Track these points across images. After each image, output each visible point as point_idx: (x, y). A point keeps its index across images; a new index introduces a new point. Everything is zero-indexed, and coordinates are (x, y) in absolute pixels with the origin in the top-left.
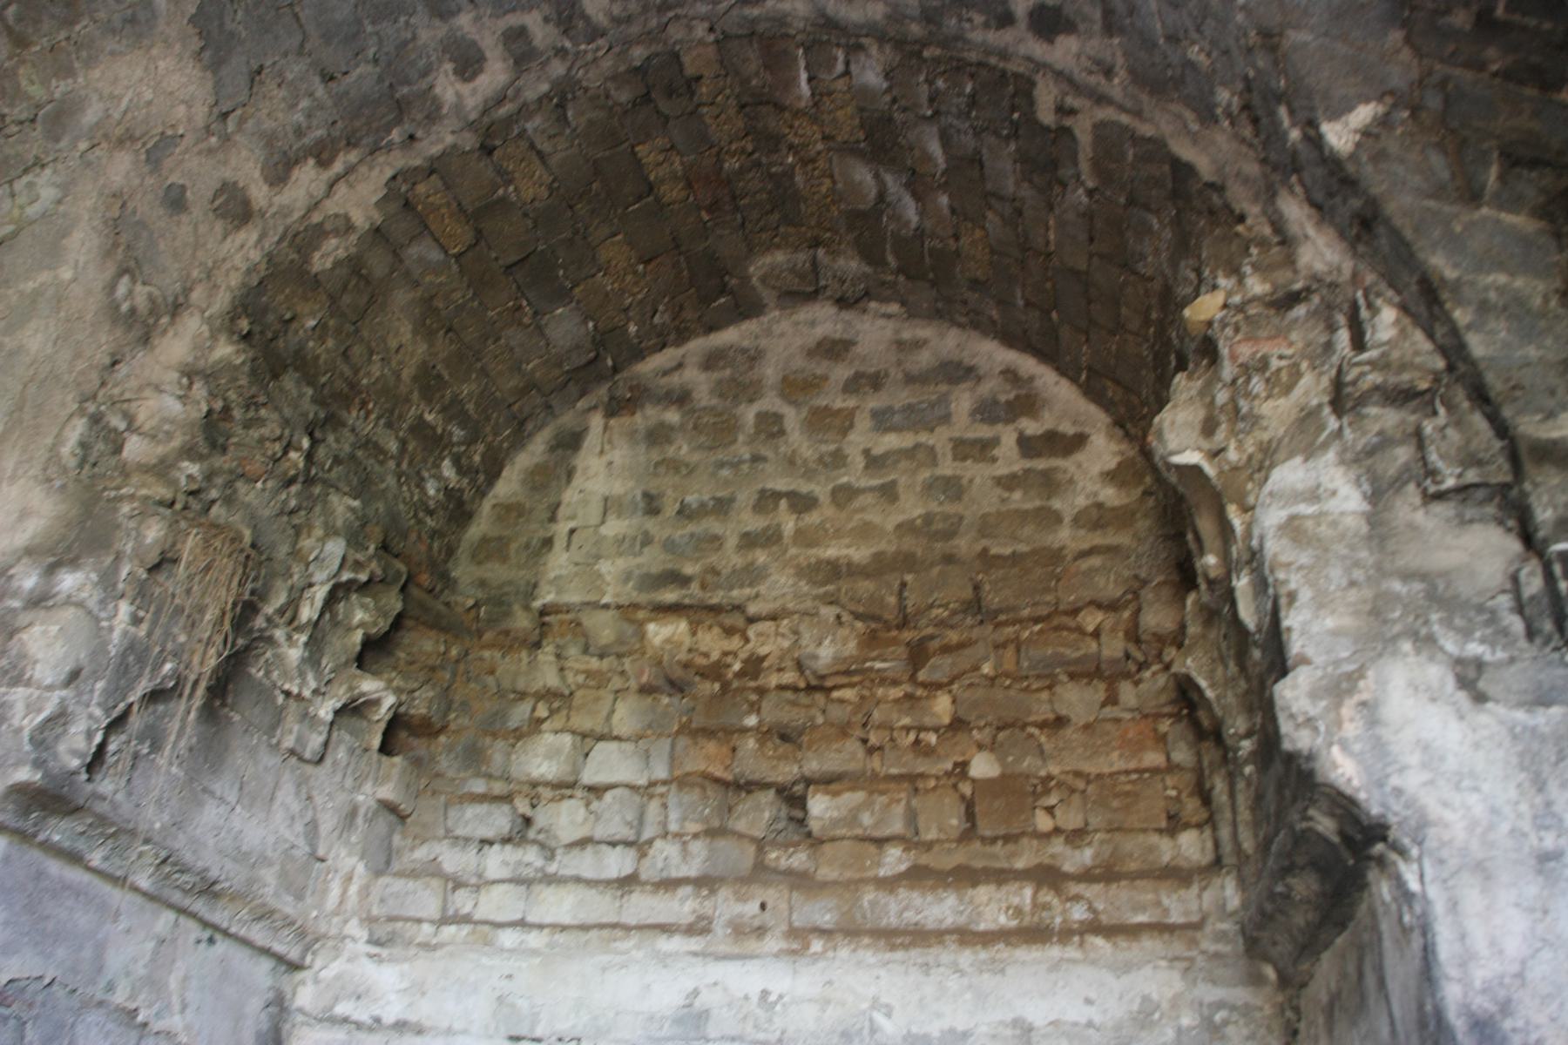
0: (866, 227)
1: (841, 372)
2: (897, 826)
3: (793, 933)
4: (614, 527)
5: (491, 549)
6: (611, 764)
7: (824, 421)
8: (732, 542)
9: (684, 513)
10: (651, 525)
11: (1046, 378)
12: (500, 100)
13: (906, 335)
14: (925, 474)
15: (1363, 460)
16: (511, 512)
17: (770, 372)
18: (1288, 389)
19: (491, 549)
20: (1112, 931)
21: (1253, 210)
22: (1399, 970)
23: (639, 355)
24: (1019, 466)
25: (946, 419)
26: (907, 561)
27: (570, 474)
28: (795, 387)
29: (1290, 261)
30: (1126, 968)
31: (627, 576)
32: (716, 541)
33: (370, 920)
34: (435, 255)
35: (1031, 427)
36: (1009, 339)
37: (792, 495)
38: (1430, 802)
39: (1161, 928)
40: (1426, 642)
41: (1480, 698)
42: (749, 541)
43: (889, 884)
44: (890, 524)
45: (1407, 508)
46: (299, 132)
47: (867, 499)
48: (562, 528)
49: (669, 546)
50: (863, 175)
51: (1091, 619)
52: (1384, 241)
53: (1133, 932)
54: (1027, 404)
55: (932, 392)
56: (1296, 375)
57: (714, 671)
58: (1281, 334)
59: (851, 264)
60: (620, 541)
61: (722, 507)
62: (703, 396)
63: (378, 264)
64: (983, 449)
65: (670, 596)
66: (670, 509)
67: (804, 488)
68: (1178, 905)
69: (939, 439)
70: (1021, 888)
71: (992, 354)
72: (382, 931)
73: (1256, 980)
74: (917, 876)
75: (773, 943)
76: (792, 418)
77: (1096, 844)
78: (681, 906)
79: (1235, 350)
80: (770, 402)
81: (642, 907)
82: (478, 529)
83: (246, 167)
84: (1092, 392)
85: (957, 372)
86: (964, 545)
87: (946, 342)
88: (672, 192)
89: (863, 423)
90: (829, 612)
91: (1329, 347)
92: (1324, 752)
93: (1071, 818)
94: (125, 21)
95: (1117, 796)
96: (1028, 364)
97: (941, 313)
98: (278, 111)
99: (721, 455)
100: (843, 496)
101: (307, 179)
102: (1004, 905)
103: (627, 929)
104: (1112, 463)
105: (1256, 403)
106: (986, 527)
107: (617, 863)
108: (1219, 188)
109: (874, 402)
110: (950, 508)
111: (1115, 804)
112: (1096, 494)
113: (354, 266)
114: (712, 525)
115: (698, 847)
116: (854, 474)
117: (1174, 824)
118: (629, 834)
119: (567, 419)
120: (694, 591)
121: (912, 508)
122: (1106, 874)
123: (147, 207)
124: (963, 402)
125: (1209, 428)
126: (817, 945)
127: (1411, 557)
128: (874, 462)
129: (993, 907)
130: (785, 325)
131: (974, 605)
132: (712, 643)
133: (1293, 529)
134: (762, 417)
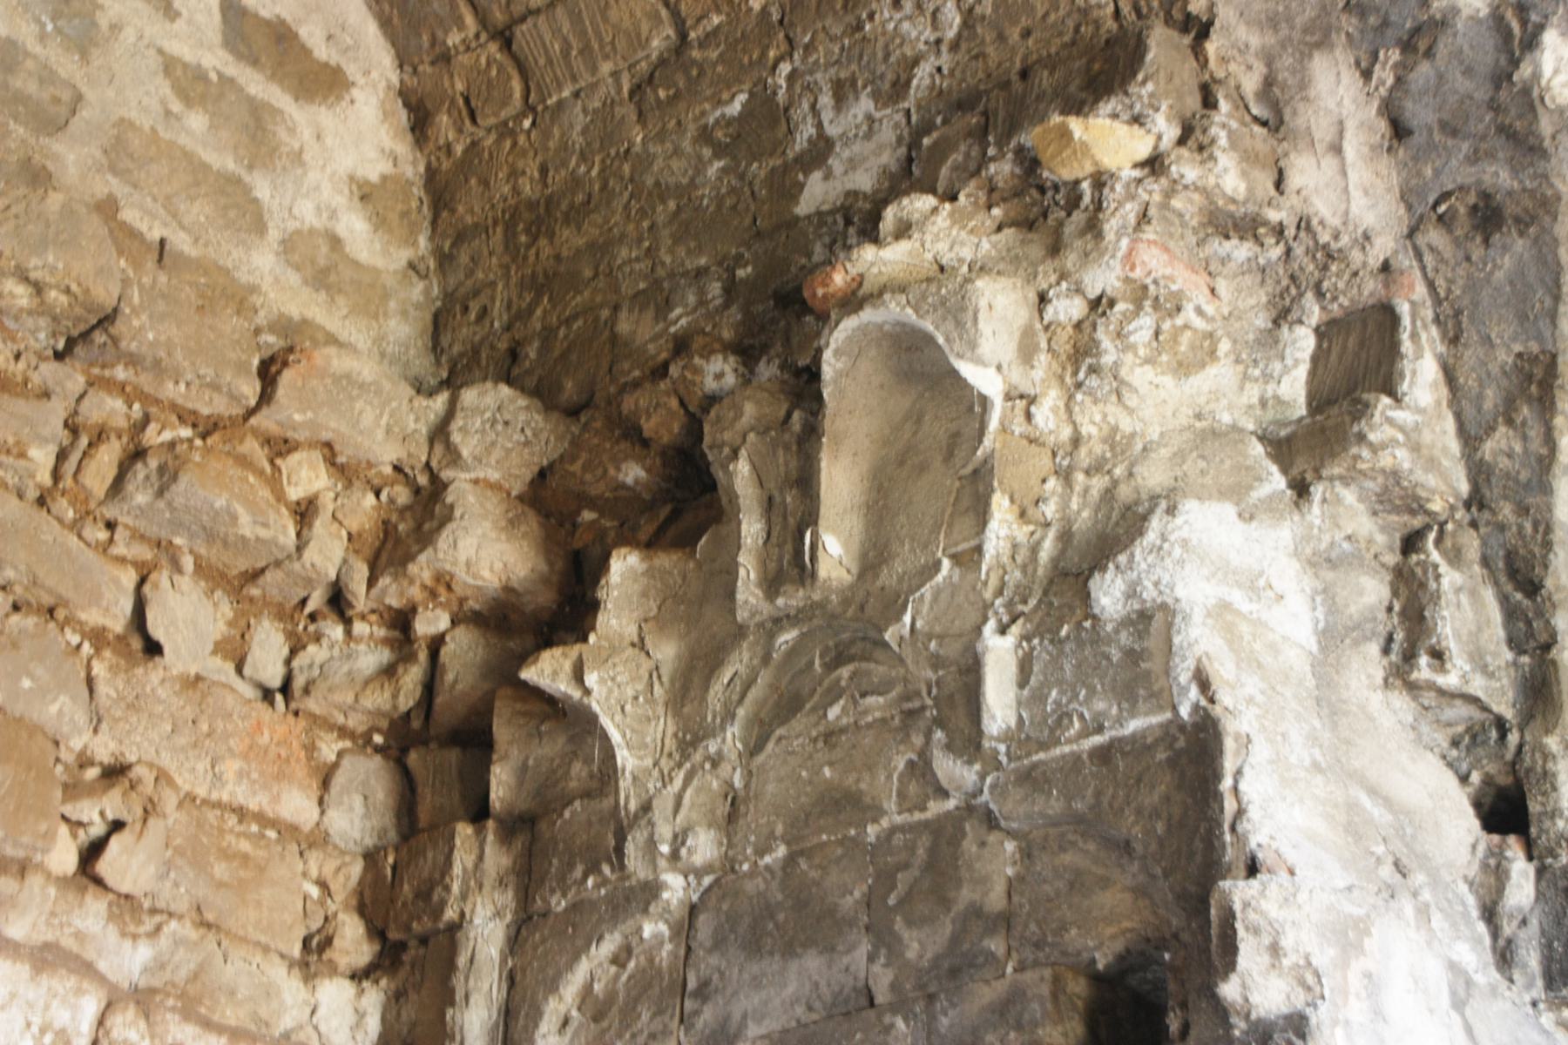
18: (1183, 369)
24: (215, 60)
51: (307, 476)
52: (1507, 261)
70: (79, 992)
77: (164, 941)
91: (1270, 340)
92: (1326, 1031)
95: (226, 855)
102: (37, 1021)
104: (375, 169)
105: (1129, 358)
111: (220, 870)
112: (333, 214)
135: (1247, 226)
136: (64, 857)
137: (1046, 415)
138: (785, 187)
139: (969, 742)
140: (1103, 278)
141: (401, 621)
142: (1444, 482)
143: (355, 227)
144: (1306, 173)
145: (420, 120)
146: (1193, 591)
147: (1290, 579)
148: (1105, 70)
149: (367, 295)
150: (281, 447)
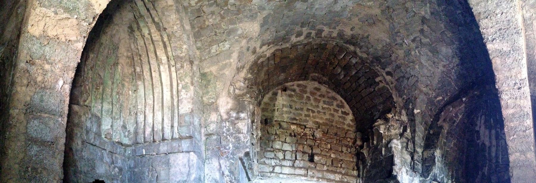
1: (319, 93)
4: (285, 109)
7: (316, 100)
8: (303, 115)
10: (291, 110)
11: (345, 104)
16: (266, 104)
17: (308, 90)
23: (287, 82)
24: (341, 115)
25: (333, 105)
27: (276, 99)
28: (312, 94)
32: (301, 115)
35: (343, 110)
36: (342, 96)
37: (311, 110)
42: (306, 116)
44: (325, 118)
49: (294, 114)
51: (349, 140)
54: (342, 106)
55: (331, 101)
57: (299, 134)
60: (286, 112)
61: (302, 109)
64: (337, 111)
65: (295, 122)
67: (314, 109)
69: (332, 107)
71: (339, 97)
75: (315, 179)
76: (312, 98)
78: (302, 172)
79: (391, 123)
80: (308, 95)
81: (298, 171)
83: (258, 44)
84: (351, 108)
85: (334, 99)
86: (334, 124)
87: (333, 94)
91: (400, 128)
94: (250, 16)
96: (344, 101)
99: (301, 101)
100: (319, 112)
101: (265, 48)
109: (323, 99)
114: (300, 112)
115: (302, 162)
116: (320, 109)
117: (353, 170)
118: (290, 159)
119: (274, 90)
120: (298, 122)
121: (328, 117)
123: (244, 50)
124: (335, 103)
125: (385, 129)
126: (320, 180)
128: (323, 108)
131: (336, 134)
135: (399, 120)
136: (340, 166)
137: (386, 133)
138: (373, 118)
139: (382, 155)
140: (390, 124)
141: (356, 147)
142: (410, 137)
143: (351, 123)
144: (402, 117)
145: (354, 115)
146: (393, 146)
147: (399, 144)
148: (389, 111)
149: (352, 126)
150: (347, 138)
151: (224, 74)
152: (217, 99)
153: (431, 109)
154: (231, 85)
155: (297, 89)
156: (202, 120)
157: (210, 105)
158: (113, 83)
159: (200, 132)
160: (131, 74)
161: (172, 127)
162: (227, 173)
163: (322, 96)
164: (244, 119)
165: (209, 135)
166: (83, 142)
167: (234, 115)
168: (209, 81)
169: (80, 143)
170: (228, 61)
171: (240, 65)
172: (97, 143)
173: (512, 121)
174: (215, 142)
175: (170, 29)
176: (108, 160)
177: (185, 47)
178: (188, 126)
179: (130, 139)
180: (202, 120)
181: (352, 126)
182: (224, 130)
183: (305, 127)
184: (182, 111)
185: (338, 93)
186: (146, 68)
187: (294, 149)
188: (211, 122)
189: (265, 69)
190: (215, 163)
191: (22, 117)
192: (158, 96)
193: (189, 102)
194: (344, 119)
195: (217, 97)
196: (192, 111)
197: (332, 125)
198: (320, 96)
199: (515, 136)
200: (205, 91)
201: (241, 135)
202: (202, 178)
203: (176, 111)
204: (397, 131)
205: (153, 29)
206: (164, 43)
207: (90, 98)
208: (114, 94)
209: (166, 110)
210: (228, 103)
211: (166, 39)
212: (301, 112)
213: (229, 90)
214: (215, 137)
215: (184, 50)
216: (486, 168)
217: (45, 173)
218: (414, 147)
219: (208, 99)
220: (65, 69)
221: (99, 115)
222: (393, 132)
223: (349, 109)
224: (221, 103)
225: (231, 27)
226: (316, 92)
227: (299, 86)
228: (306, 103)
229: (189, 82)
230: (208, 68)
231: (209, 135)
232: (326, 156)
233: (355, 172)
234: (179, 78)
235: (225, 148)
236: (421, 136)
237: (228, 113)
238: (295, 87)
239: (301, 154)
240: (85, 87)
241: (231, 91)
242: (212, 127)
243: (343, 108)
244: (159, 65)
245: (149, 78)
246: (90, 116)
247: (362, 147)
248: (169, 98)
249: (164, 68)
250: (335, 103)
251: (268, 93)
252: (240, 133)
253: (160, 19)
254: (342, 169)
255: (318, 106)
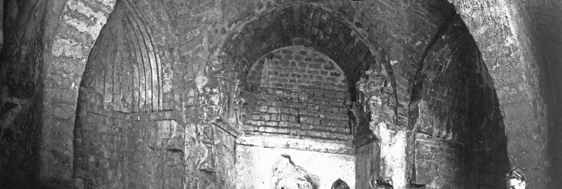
0: (314, 38)
1: (305, 57)
2: (312, 123)
3: (300, 136)
4: (271, 76)
5: (252, 78)
6: (272, 110)
7: (301, 64)
9: (281, 75)
10: (276, 77)
11: (335, 64)
12: (263, 12)
13: (315, 53)
14: (316, 75)
15: (382, 99)
16: (253, 72)
17: (293, 55)
19: (252, 78)
20: (339, 139)
21: (378, 63)
22: (375, 152)
23: (273, 49)
25: (320, 68)
26: (314, 87)
27: (263, 67)
28: (297, 58)
29: (380, 72)
30: (339, 144)
31: (273, 84)
32: (286, 80)
33: (244, 131)
34: (249, 36)
35: (333, 71)
36: (331, 58)
38: (382, 138)
39: (344, 140)
40: (385, 122)
41: (388, 128)
42: (291, 81)
43: (312, 130)
45: (386, 106)
46: (234, 19)
47: (308, 77)
48: (263, 76)
49: (279, 80)
50: (317, 31)
51: (339, 100)
53: (341, 140)
54: (332, 68)
56: (377, 85)
57: (286, 99)
58: (377, 79)
59: (309, 41)
60: (272, 78)
61: (287, 75)
62: (283, 58)
63: (240, 38)
65: (280, 87)
66: (279, 74)
68: (346, 137)
69: (319, 70)
71: (327, 58)
72: (247, 132)
73: (353, 147)
74: (314, 129)
75: (298, 137)
78: (285, 131)
79: (371, 79)
80: (293, 60)
81: (281, 131)
82: (250, 75)
83: (226, 25)
84: (342, 68)
85: (322, 60)
86: (322, 86)
87: (322, 55)
88: (285, 27)
89: (308, 66)
90: (303, 93)
91: (382, 83)
93: (333, 125)
96: (333, 62)
97: (321, 51)
98: (231, 16)
103: (280, 133)
104: (343, 79)
106: (325, 84)
107: (274, 124)
108: (374, 57)
110: (320, 81)
113: (237, 38)
117: (346, 127)
118: (276, 120)
119: (261, 59)
121: (315, 80)
122: (337, 132)
123: (213, 33)
124: (323, 65)
125: (365, 87)
127: (385, 111)
128: (309, 72)
129: (324, 135)
130: (296, 48)
131: (324, 96)
132: (286, 95)
133: (373, 104)
134: (292, 62)
143: (342, 84)
147: (379, 100)
149: (344, 87)
151: (198, 57)
152: (194, 78)
153: (412, 57)
154: (207, 64)
155: (283, 56)
156: (183, 96)
157: (189, 83)
158: (113, 67)
159: (181, 106)
160: (128, 58)
161: (159, 102)
162: (202, 133)
163: (308, 59)
164: (216, 93)
165: (188, 107)
166: (88, 112)
167: (209, 90)
168: (187, 63)
169: (85, 112)
170: (200, 45)
171: (211, 46)
172: (100, 112)
173: (489, 44)
174: (193, 112)
175: (151, 24)
176: (110, 123)
177: (164, 38)
178: (169, 102)
179: (128, 109)
180: (183, 96)
181: (344, 87)
182: (201, 102)
183: (291, 92)
184: (165, 91)
185: (326, 54)
186: (139, 55)
187: (280, 112)
188: (190, 97)
189: (243, 42)
190: (193, 127)
191: (50, 106)
192: (149, 78)
193: (170, 84)
194: (334, 80)
195: (195, 76)
196: (172, 90)
197: (320, 88)
198: (306, 60)
199: (498, 65)
200: (185, 72)
201: (213, 107)
202: (183, 137)
203: (161, 90)
204: (378, 87)
205: (140, 23)
206: (148, 34)
207: (94, 81)
208: (115, 75)
209: (154, 89)
210: (204, 80)
211: (149, 32)
212: (286, 78)
213: (205, 69)
214: (193, 108)
215: (163, 40)
216: (492, 115)
217: (64, 135)
218: (397, 101)
219: (188, 78)
220: (76, 76)
221: (102, 93)
222: (374, 88)
223: (340, 70)
224: (198, 81)
225: (198, 15)
226: (302, 56)
227: (284, 52)
228: (292, 69)
229: (170, 67)
230: (186, 51)
231: (188, 107)
232: (313, 116)
233: (347, 129)
234: (163, 64)
235: (201, 117)
236: (405, 88)
237: (204, 89)
238: (281, 53)
239: (287, 117)
240: (90, 73)
241: (207, 70)
242: (191, 100)
243: (333, 70)
244: (148, 53)
245: (141, 63)
246: (94, 94)
247: (351, 106)
248: (156, 79)
249: (151, 55)
250: (323, 65)
251: (254, 62)
252: (213, 105)
253: (143, 16)
254: (331, 128)
255: (304, 71)
